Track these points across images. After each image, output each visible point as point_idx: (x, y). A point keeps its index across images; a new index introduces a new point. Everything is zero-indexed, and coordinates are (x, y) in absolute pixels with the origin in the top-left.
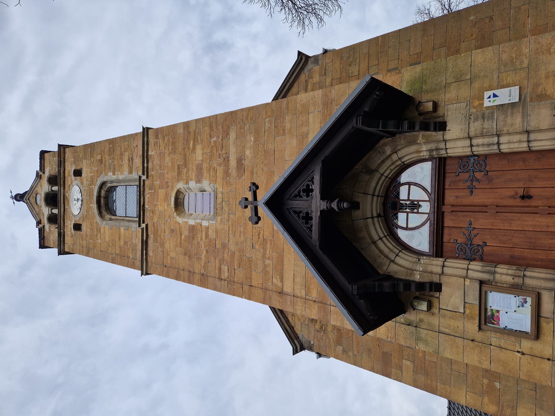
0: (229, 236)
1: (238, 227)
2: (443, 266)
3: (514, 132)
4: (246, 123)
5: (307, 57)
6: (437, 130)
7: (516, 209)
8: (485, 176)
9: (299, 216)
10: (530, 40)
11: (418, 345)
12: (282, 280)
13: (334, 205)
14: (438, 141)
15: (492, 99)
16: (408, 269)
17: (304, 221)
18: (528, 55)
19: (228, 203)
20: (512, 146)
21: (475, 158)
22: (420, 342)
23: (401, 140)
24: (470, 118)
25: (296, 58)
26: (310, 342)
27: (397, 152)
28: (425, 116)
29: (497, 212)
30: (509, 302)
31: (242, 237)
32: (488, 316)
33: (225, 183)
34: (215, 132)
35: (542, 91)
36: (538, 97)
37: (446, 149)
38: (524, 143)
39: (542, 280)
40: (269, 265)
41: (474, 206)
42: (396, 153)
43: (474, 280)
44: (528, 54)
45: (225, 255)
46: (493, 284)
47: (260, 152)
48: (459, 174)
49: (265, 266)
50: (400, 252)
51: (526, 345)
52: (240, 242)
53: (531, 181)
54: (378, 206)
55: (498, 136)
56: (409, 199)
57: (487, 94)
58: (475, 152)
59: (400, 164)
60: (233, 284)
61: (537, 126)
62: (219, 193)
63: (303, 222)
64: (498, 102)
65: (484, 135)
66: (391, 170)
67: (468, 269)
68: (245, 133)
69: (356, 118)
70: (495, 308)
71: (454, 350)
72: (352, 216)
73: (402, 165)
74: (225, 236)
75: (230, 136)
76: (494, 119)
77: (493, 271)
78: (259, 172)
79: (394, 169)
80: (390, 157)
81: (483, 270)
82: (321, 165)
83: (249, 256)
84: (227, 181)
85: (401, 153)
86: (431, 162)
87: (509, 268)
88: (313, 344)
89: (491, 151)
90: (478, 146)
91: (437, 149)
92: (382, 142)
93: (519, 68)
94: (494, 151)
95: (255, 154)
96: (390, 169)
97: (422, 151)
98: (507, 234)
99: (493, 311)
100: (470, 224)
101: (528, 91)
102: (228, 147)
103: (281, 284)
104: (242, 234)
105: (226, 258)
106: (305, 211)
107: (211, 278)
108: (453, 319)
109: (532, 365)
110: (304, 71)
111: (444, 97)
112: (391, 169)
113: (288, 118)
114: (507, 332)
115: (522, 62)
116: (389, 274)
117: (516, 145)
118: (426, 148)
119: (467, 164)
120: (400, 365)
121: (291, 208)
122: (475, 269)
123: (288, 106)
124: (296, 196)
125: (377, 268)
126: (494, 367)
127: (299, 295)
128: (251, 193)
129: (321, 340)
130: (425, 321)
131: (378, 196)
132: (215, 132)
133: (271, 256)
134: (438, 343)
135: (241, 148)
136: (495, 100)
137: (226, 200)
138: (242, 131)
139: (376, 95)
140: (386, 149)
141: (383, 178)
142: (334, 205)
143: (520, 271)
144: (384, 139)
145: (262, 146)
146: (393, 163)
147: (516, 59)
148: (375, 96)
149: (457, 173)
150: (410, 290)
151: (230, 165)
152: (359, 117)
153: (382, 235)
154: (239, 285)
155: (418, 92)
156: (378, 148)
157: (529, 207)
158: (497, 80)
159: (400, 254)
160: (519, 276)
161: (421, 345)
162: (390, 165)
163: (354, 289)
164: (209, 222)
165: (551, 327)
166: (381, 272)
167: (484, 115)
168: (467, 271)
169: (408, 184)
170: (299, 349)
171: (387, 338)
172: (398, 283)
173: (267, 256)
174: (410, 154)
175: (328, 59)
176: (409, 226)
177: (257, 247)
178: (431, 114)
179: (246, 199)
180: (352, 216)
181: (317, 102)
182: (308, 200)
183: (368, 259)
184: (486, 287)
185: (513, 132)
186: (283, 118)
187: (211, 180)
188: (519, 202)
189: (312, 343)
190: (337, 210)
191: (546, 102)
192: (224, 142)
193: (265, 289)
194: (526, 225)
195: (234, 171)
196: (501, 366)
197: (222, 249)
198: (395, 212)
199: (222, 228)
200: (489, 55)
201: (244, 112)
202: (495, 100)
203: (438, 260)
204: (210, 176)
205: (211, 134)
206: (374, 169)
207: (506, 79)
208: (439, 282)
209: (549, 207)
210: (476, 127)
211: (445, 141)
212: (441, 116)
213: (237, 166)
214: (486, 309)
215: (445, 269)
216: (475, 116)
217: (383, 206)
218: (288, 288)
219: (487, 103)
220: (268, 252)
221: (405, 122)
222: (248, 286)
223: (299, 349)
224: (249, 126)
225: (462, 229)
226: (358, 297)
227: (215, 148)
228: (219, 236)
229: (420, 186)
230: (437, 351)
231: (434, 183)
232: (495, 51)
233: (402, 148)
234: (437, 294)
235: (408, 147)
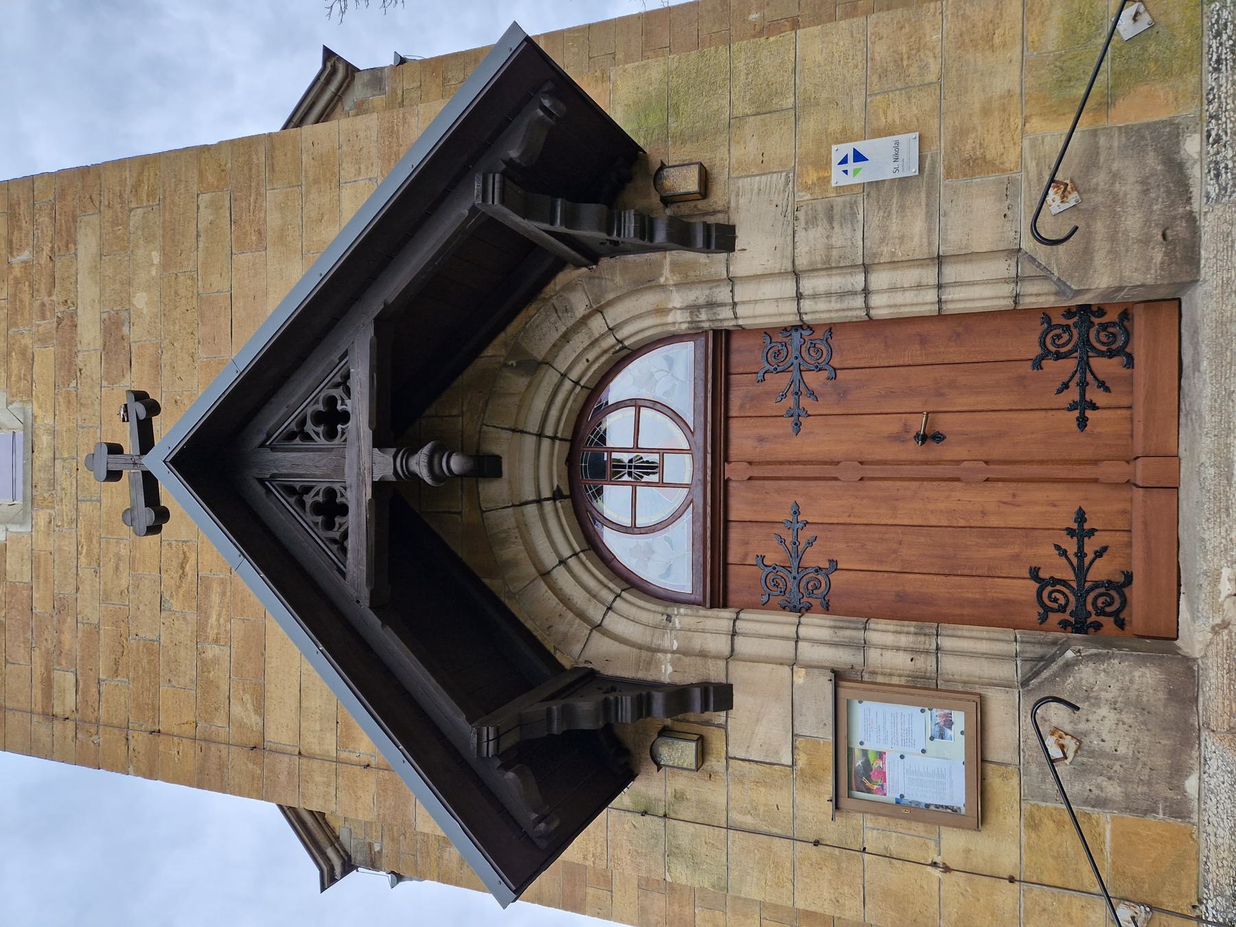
0: (79, 572)
1: (108, 543)
2: (734, 634)
3: (907, 258)
4: (133, 205)
5: (351, 70)
6: (713, 247)
7: (907, 470)
8: (830, 383)
9: (302, 504)
10: (944, 9)
11: (672, 870)
12: (260, 707)
13: (419, 464)
14: (713, 282)
15: (851, 166)
16: (640, 647)
17: (320, 519)
18: (938, 50)
19: (75, 465)
20: (900, 298)
21: (803, 332)
22: (676, 861)
23: (614, 271)
24: (796, 219)
25: (319, 66)
26: (370, 846)
27: (605, 311)
28: (679, 207)
29: (861, 479)
30: (907, 726)
31: (125, 574)
32: (855, 771)
33: (61, 400)
34: (26, 235)
35: (974, 149)
36: (964, 166)
37: (734, 304)
38: (929, 291)
39: (982, 660)
40: (216, 661)
41: (805, 463)
42: (602, 313)
43: (816, 671)
44: (940, 47)
45: (67, 638)
46: (866, 677)
47: (183, 301)
48: (766, 375)
49: (204, 666)
50: (618, 599)
51: (954, 843)
52: (117, 590)
53: (942, 395)
54: (555, 468)
55: (866, 269)
56: (637, 448)
57: (840, 151)
58: (806, 314)
59: (613, 347)
60: (93, 730)
61: (964, 242)
62: (40, 432)
63: (316, 524)
64: (861, 174)
65: (833, 265)
66: (586, 364)
67: (797, 639)
68: (129, 239)
69: (481, 178)
70: (872, 746)
71: (769, 875)
72: (479, 497)
73: (617, 348)
74: (66, 573)
75: (80, 247)
76: (858, 221)
77: (861, 639)
78: (180, 363)
79: (597, 358)
80: (586, 324)
81: (835, 639)
82: (370, 333)
83: (150, 636)
84: (68, 393)
85: (615, 314)
86: (693, 343)
87: (898, 629)
88: (380, 852)
89: (846, 313)
90: (815, 296)
91: (711, 305)
92: (562, 278)
93: (918, 83)
94: (855, 313)
95: (165, 305)
96: (585, 361)
97: (671, 310)
98: (887, 536)
99: (867, 754)
100: (795, 513)
101: (940, 147)
102: (72, 281)
103: (259, 720)
104: (124, 567)
105: (67, 647)
106: (323, 486)
107: (18, 715)
108: (765, 784)
109: (971, 899)
110: (342, 104)
111: (727, 156)
112: (588, 361)
113: (272, 196)
114: (905, 810)
115: (924, 68)
116: (590, 666)
117: (909, 297)
118: (680, 300)
119: (785, 350)
120: (608, 876)
121: (273, 476)
122: (816, 637)
123: (272, 158)
124: (291, 436)
125: (555, 649)
126: (873, 913)
127: (316, 749)
128: (131, 428)
129: (402, 838)
130: (688, 797)
131: (554, 438)
132: (26, 235)
133: (225, 630)
134: (725, 859)
135: (117, 286)
136: (860, 169)
137: (66, 455)
138: (119, 233)
139: (544, 108)
140: (573, 301)
141: (568, 385)
142: (418, 464)
143: (927, 638)
144: (567, 271)
145: (189, 282)
146: (593, 344)
147: (909, 58)
148: (541, 113)
149: (761, 374)
150: (649, 713)
151: (78, 339)
152: (491, 175)
153: (566, 552)
154: (116, 731)
155: (658, 139)
156: (551, 297)
157: (938, 462)
158: (863, 116)
159: (618, 604)
160: (927, 652)
161: (679, 867)
162: (585, 349)
163: (485, 739)
164: (7, 530)
165: (1013, 789)
166: (567, 663)
167: (832, 211)
168: (797, 642)
169: (633, 403)
170: (338, 870)
171: (585, 858)
172: (616, 699)
173: (212, 633)
174: (640, 316)
175: (408, 83)
176: (639, 523)
177: (176, 605)
178: (692, 204)
179: (115, 449)
180: (481, 498)
181: (364, 150)
182: (330, 450)
183: (529, 625)
184: (852, 688)
185: (904, 259)
186: (258, 194)
187: (14, 390)
188: (913, 450)
189: (376, 850)
190: (428, 480)
191: (984, 179)
192: (58, 264)
193: (205, 740)
194: (932, 512)
195: (95, 360)
196: (893, 911)
197: (55, 619)
198: (597, 481)
199: (51, 549)
200: (842, 44)
201: (125, 171)
202: (860, 169)
203: (718, 618)
204: (8, 378)
205: (14, 241)
206: (540, 358)
207: (885, 113)
208: (724, 681)
209: (986, 462)
210: (811, 243)
211: (731, 280)
212: (719, 209)
213: (105, 345)
214: (850, 751)
215: (739, 641)
216: (810, 212)
217: (567, 468)
218: (280, 732)
219: (837, 178)
220: (213, 620)
221: (627, 215)
222: (145, 734)
223: (338, 870)
224: (144, 217)
225: (776, 525)
226: (498, 763)
227: (27, 284)
228: (42, 574)
229: (665, 410)
230: (723, 884)
231: (701, 401)
232: (855, 35)
233: (619, 299)
234: (720, 717)
235: (632, 298)
